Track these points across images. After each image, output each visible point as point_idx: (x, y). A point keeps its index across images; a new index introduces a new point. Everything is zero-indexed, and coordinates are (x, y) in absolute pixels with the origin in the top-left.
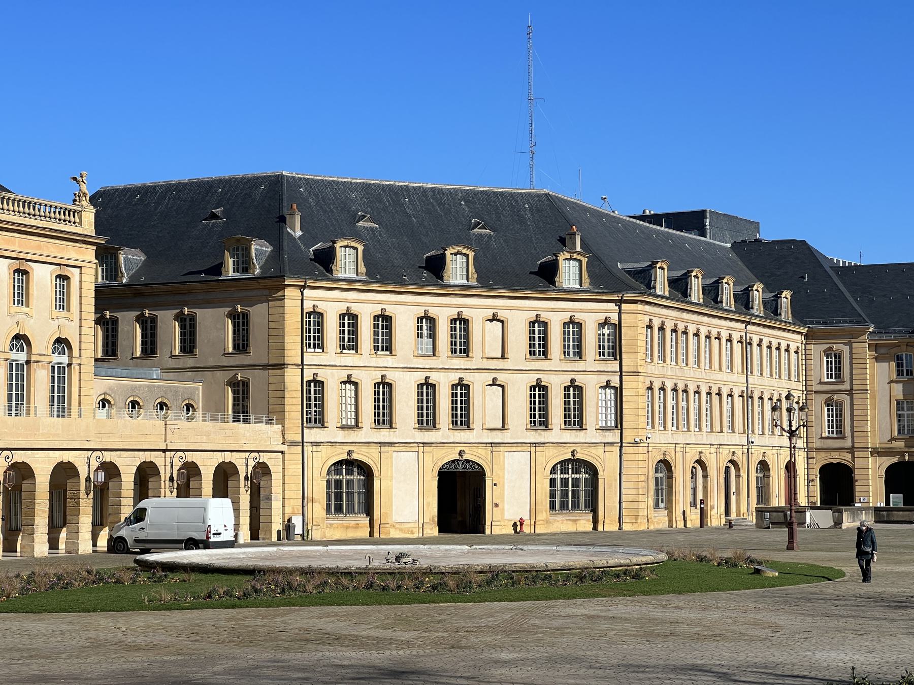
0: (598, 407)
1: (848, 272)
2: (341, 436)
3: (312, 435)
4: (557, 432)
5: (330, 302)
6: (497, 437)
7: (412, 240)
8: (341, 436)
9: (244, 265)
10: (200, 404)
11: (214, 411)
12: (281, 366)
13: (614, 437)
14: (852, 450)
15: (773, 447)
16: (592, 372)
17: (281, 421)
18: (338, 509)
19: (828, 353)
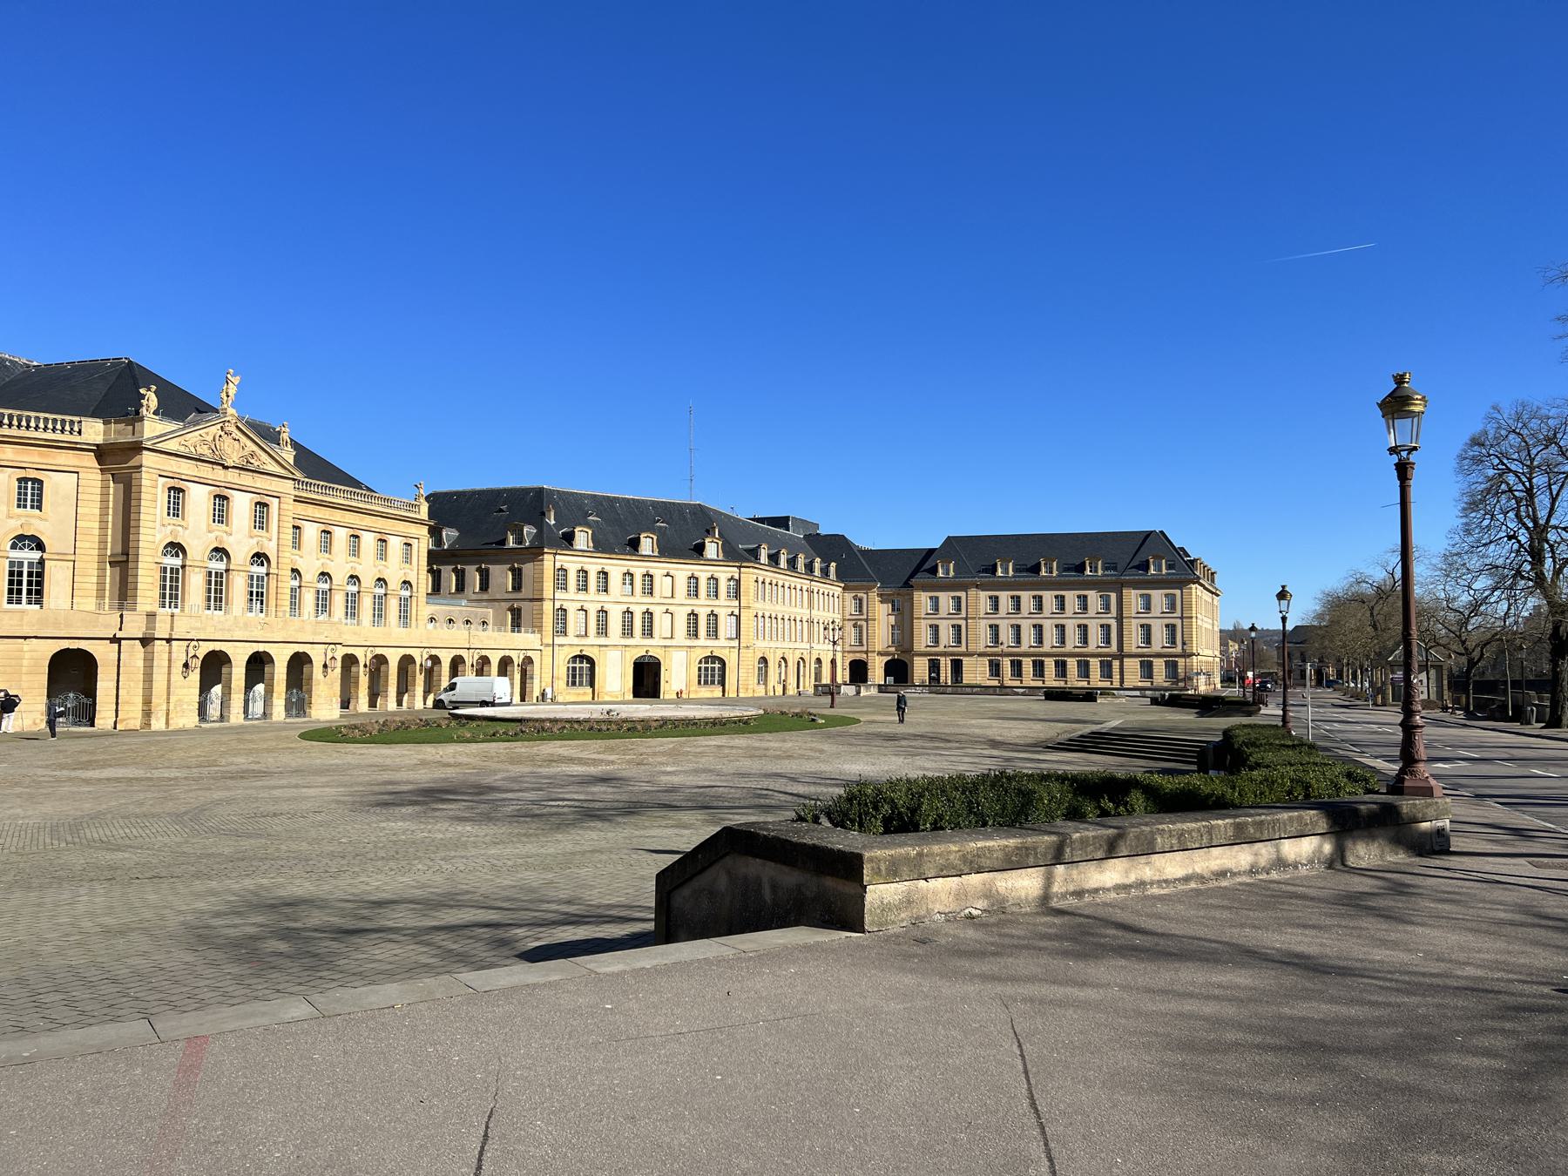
0: (726, 626)
1: (867, 553)
2: (577, 641)
3: (559, 640)
4: (703, 640)
5: (571, 563)
6: (668, 643)
7: (621, 527)
8: (577, 641)
9: (520, 540)
10: (491, 622)
11: (500, 624)
12: (541, 600)
13: (735, 643)
14: (867, 652)
15: (824, 650)
16: (724, 606)
17: (540, 631)
18: (574, 684)
19: (855, 598)
